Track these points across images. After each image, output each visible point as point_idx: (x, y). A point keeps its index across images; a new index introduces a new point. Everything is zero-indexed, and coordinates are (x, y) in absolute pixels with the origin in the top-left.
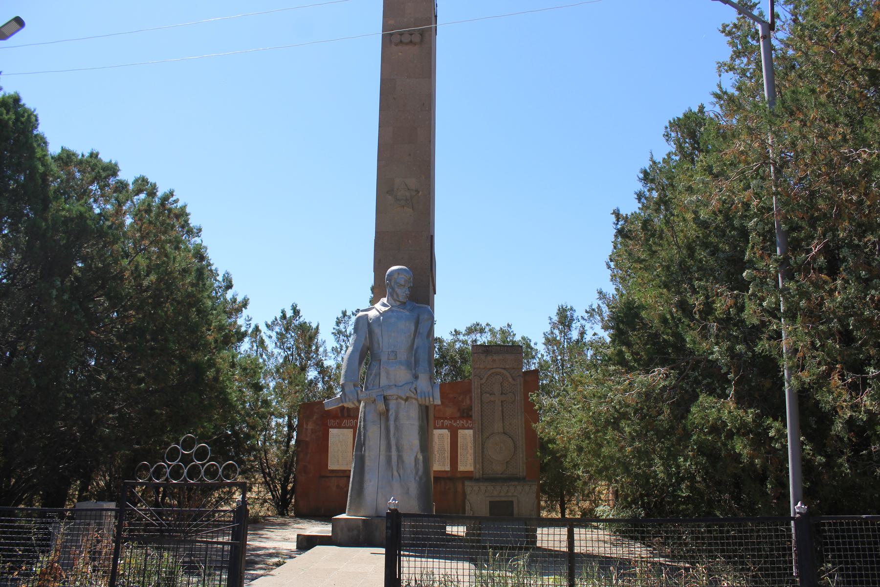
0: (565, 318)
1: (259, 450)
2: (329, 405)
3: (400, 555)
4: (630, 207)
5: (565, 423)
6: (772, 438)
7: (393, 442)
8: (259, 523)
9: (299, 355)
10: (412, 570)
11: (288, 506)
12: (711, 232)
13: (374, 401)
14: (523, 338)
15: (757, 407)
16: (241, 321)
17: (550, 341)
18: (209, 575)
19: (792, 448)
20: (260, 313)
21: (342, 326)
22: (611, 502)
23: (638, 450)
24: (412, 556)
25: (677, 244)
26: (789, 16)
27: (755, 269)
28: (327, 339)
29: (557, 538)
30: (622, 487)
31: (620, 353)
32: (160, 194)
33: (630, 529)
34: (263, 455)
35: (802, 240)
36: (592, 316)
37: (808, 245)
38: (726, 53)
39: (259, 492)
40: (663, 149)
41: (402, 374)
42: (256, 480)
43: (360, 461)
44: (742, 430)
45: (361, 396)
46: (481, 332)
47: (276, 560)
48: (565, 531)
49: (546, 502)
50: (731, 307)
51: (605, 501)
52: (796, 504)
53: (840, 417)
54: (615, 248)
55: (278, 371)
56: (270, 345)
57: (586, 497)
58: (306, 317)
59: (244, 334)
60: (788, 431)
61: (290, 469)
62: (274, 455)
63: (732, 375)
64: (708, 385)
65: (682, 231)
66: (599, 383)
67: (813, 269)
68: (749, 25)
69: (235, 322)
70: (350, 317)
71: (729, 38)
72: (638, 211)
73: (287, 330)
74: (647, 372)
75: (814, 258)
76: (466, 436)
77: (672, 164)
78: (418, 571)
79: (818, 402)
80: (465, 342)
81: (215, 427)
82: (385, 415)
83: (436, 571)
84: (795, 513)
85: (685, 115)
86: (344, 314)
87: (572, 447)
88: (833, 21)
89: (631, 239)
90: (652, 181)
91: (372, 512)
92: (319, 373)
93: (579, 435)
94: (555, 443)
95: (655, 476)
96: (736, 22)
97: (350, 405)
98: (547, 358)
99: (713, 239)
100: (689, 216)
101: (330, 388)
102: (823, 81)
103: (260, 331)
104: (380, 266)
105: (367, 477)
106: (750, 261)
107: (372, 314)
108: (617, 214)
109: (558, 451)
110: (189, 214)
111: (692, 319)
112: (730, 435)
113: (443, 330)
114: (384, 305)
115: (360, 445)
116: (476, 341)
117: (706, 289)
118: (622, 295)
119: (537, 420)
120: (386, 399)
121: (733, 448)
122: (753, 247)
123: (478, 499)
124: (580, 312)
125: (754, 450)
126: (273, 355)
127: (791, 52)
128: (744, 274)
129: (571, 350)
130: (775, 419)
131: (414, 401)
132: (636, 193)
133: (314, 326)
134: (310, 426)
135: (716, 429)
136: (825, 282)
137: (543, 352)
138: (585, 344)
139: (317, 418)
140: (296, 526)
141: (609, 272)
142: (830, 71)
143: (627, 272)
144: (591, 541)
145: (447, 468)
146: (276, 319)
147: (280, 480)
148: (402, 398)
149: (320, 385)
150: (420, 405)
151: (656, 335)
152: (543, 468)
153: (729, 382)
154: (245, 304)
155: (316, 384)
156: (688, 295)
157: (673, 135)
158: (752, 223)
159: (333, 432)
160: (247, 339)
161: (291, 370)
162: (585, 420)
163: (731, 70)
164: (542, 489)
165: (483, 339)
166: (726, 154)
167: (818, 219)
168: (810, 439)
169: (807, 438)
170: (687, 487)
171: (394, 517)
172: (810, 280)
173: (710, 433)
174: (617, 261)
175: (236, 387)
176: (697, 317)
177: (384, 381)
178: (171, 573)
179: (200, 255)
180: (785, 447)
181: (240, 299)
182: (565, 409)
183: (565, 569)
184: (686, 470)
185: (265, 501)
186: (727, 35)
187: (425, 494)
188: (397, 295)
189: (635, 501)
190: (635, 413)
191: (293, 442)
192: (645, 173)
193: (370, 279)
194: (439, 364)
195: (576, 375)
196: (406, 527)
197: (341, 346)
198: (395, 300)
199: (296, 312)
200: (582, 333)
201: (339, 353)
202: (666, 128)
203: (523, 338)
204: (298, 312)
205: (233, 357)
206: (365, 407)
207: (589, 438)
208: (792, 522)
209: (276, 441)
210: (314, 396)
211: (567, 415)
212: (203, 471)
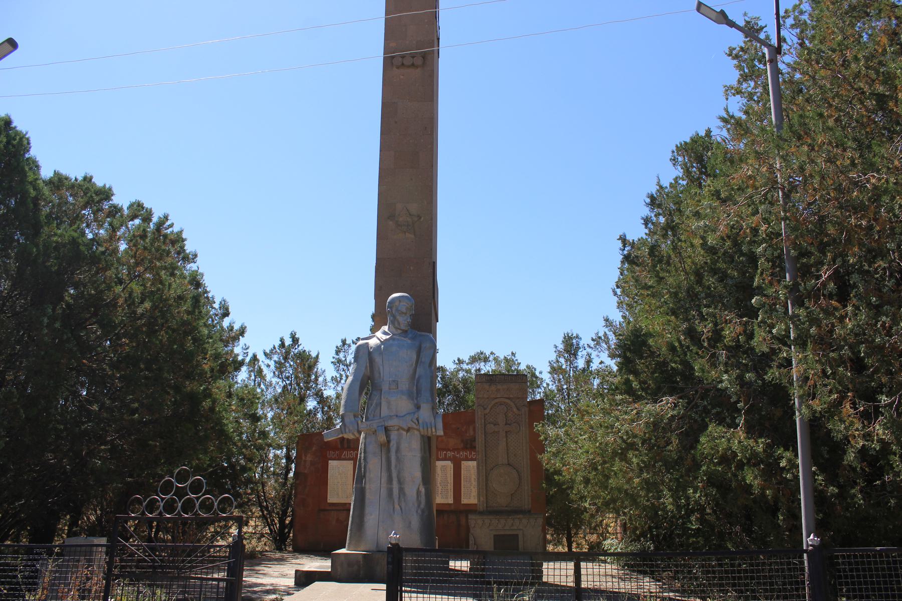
0: (570, 346)
1: (256, 483)
2: (329, 436)
3: (401, 591)
4: (637, 232)
5: (572, 451)
6: (784, 468)
7: (394, 475)
8: (256, 559)
9: (298, 385)
11: (287, 541)
12: (719, 258)
13: (375, 432)
14: (528, 367)
15: (768, 437)
16: (237, 350)
17: (555, 370)
19: (804, 479)
20: (258, 341)
21: (341, 355)
23: (646, 481)
24: (414, 592)
25: (684, 270)
26: (796, 40)
28: (326, 368)
29: (563, 572)
30: (630, 519)
31: (627, 382)
34: (260, 488)
35: (812, 266)
36: (598, 344)
37: (818, 271)
38: (732, 76)
39: (256, 526)
40: (670, 174)
41: (403, 405)
42: (253, 513)
44: (753, 460)
45: (362, 426)
49: (552, 535)
50: (740, 334)
53: (852, 447)
54: (622, 274)
55: (276, 400)
56: (269, 374)
57: (594, 530)
58: (307, 345)
59: (242, 363)
60: (799, 461)
61: (288, 502)
62: (272, 488)
64: (718, 414)
67: (824, 295)
68: (756, 49)
69: (232, 351)
70: (349, 346)
71: (735, 62)
72: (644, 237)
73: (286, 358)
74: (655, 402)
75: (824, 284)
76: (470, 467)
79: (830, 431)
80: (468, 371)
84: (808, 545)
85: (692, 139)
86: (344, 342)
87: (579, 478)
88: (839, 45)
89: (637, 265)
90: (659, 206)
91: (373, 547)
92: (318, 403)
93: (585, 467)
94: (561, 475)
96: (743, 45)
97: (351, 437)
98: (553, 387)
99: (721, 265)
100: (697, 242)
102: (831, 106)
103: (258, 361)
104: (381, 293)
105: (368, 509)
106: (759, 287)
107: (373, 342)
108: (623, 240)
109: (564, 483)
110: (185, 240)
111: (701, 347)
112: (741, 466)
113: (445, 359)
114: (385, 333)
115: (360, 478)
116: (479, 370)
118: (629, 323)
119: (542, 451)
120: (387, 430)
121: (744, 479)
122: (762, 273)
123: (483, 533)
124: (586, 340)
125: (765, 481)
126: (271, 385)
127: (798, 76)
128: (753, 301)
129: (577, 379)
130: (786, 449)
131: (416, 432)
132: (642, 218)
133: (314, 355)
134: (309, 458)
135: (726, 459)
136: (836, 309)
137: (548, 381)
139: (316, 449)
140: (294, 561)
141: (616, 299)
142: (837, 95)
143: (633, 299)
146: (274, 347)
147: (278, 513)
148: (403, 429)
149: (319, 416)
150: (422, 436)
151: (665, 364)
152: (549, 500)
153: (739, 411)
154: (242, 331)
155: (315, 415)
156: (697, 322)
157: (680, 159)
159: (332, 464)
160: (244, 369)
161: (292, 401)
162: (591, 451)
163: (738, 93)
164: (548, 522)
166: (733, 178)
168: (822, 469)
170: (697, 519)
171: (396, 552)
172: (820, 306)
173: (719, 464)
174: (623, 288)
175: (232, 417)
176: (706, 344)
177: (385, 411)
179: (196, 281)
180: (796, 478)
181: (236, 327)
184: (696, 502)
185: (262, 535)
186: (734, 58)
188: (399, 324)
189: (643, 534)
190: (643, 444)
191: (291, 475)
192: (652, 197)
193: (369, 306)
194: (441, 393)
195: (582, 405)
196: (408, 562)
197: (341, 375)
198: (396, 328)
199: (295, 340)
200: (589, 362)
201: (338, 382)
202: (673, 152)
203: (528, 367)
204: (298, 340)
205: (230, 387)
206: (365, 438)
207: (596, 469)
208: (805, 555)
209: (274, 473)
211: (573, 446)
212: (197, 505)
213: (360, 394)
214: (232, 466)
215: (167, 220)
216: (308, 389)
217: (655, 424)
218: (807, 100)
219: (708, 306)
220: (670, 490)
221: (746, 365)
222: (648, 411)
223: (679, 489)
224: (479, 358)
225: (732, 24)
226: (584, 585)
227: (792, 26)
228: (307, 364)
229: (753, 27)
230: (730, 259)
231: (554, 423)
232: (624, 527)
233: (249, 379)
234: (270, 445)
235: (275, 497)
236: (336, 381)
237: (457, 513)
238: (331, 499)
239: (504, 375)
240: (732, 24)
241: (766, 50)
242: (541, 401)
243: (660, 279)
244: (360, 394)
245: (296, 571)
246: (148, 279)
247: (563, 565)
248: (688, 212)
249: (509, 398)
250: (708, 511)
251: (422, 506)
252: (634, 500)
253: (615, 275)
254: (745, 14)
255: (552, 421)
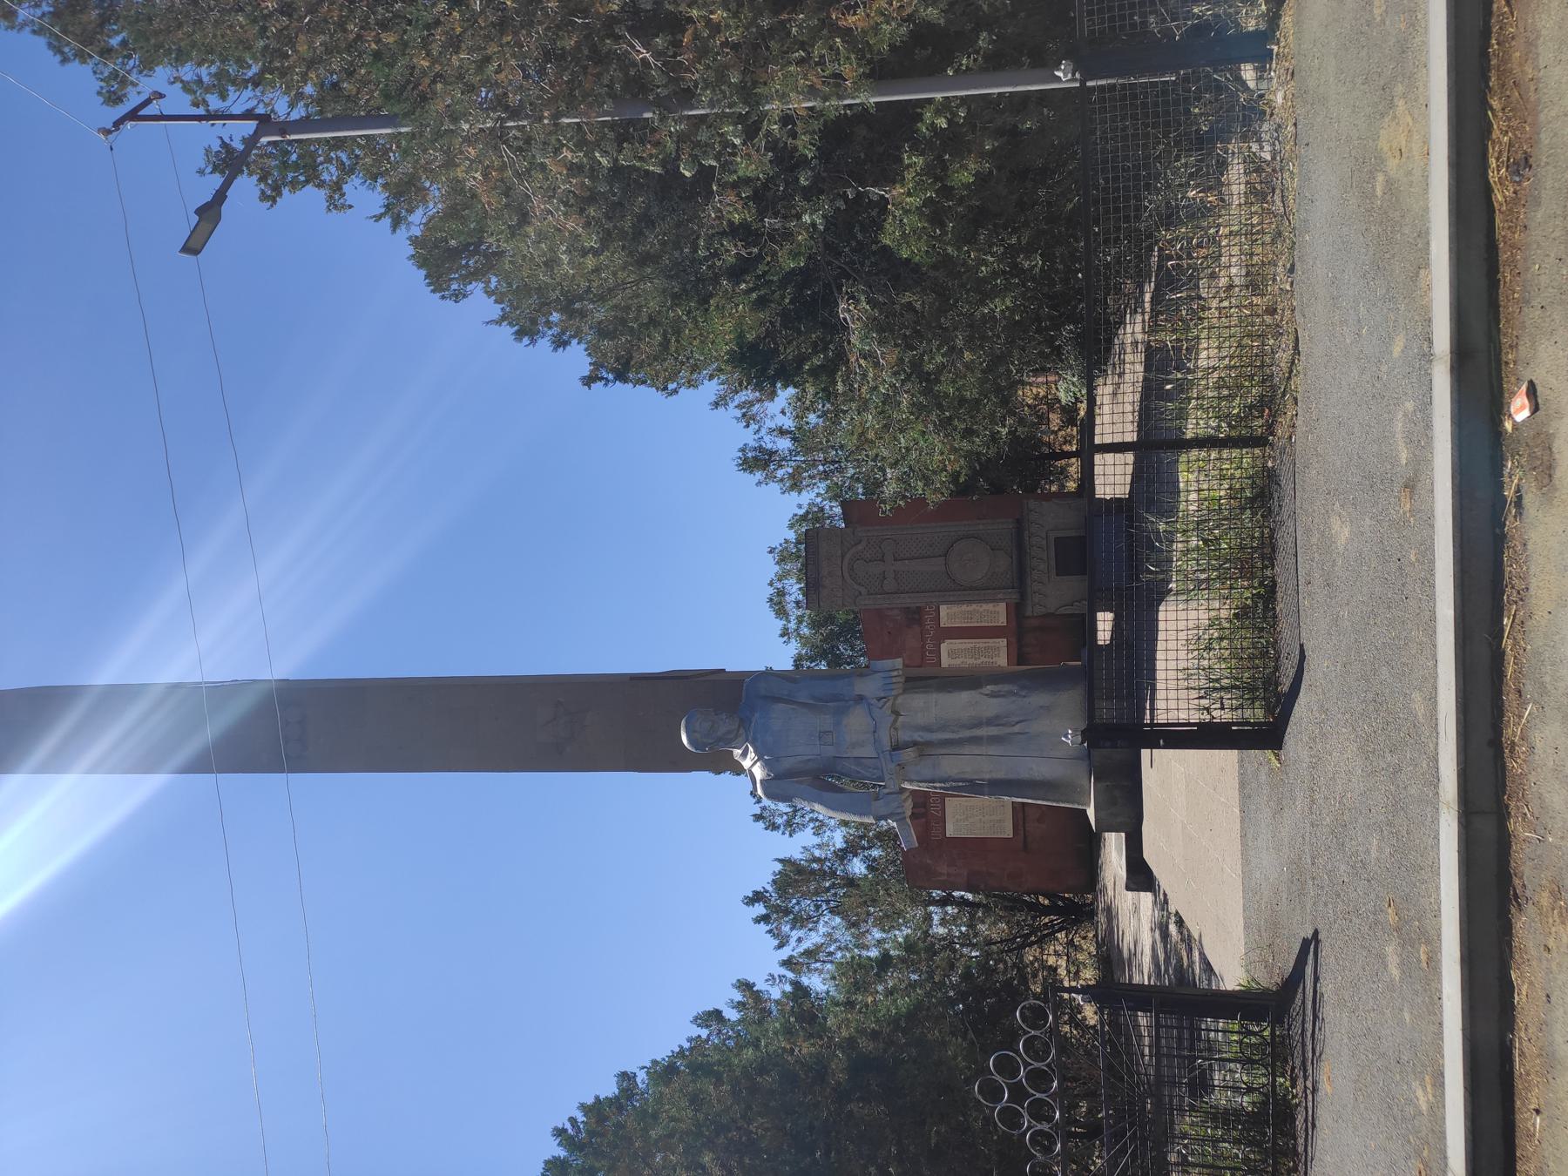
0: (758, 461)
1: (988, 955)
2: (909, 839)
3: (1152, 725)
4: (577, 358)
5: (924, 457)
6: (949, 122)
7: (967, 733)
8: (1110, 958)
9: (828, 889)
10: (1183, 705)
11: (1078, 905)
12: (615, 227)
13: (901, 766)
14: (791, 526)
15: (899, 148)
16: (776, 993)
17: (795, 484)
18: (1210, 1050)
19: (967, 89)
20: (759, 959)
21: (779, 821)
22: (1051, 378)
23: (969, 341)
24: (1152, 704)
25: (637, 283)
26: (248, 93)
27: (678, 158)
28: (799, 845)
29: (1110, 470)
30: (1028, 363)
31: (814, 372)
32: (561, 1153)
33: (1096, 355)
34: (994, 948)
35: (626, 74)
36: (753, 418)
37: (634, 64)
38: (313, 196)
39: (1056, 953)
40: (480, 304)
41: (856, 722)
42: (1036, 959)
43: (998, 787)
44: (937, 172)
45: (892, 787)
46: (783, 594)
47: (1173, 928)
48: (1098, 458)
49: (1052, 482)
50: (738, 195)
51: (1049, 388)
52: (1058, 79)
53: (916, 11)
54: (644, 382)
55: (854, 925)
56: (814, 939)
57: (1043, 419)
58: (763, 878)
59: (797, 985)
60: (938, 96)
61: (1014, 900)
62: (993, 929)
63: (849, 192)
64: (863, 229)
65: (615, 274)
66: (864, 406)
67: (675, 56)
68: (261, 156)
69: (777, 1002)
70: (764, 808)
71: (285, 191)
72: (583, 346)
73: (787, 912)
74: (846, 329)
75: (657, 55)
76: (949, 615)
77: (504, 287)
78: (1183, 694)
79: (892, 47)
80: (800, 620)
81: (953, 1034)
82: (923, 748)
83: (1182, 665)
84: (1073, 80)
85: (420, 267)
86: (758, 818)
87: (965, 445)
88: (255, 21)
89: (631, 358)
90: (534, 322)
91: (1082, 768)
92: (856, 855)
93: (946, 436)
94: (959, 473)
95: (1012, 310)
96: (255, 178)
97: (909, 804)
98: (822, 487)
99: (627, 225)
100: (590, 262)
101: (879, 836)
102: (359, 37)
103: (791, 957)
104: (680, 762)
105: (1025, 775)
106: (663, 163)
107: (758, 772)
108: (588, 381)
109: (971, 468)
110: (597, 1098)
111: (760, 258)
112: (946, 191)
113: (781, 656)
114: (744, 754)
115: (973, 787)
116: (797, 603)
117: (710, 238)
118: (720, 370)
119: (922, 501)
120: (897, 747)
121: (967, 186)
122: (641, 159)
123: (1054, 593)
124: (748, 437)
125: (970, 152)
126: (830, 934)
127: (309, 89)
128: (687, 174)
129: (808, 450)
130: (920, 118)
131: (899, 700)
132: (555, 349)
133: (779, 867)
134: (943, 869)
135: (934, 214)
136: (696, 36)
137: (813, 495)
138: (799, 428)
139: (928, 860)
140: (1110, 892)
141: (682, 390)
142: (341, 26)
143: (682, 363)
144: (1116, 417)
145: (1003, 642)
146: (770, 931)
147: (1034, 918)
148: (895, 721)
149: (875, 853)
150: (905, 691)
151: (784, 314)
152: (998, 489)
153: (859, 195)
154: (745, 986)
155: (875, 860)
156: (719, 263)
157: (454, 286)
158: (604, 161)
159: (950, 831)
160: (805, 981)
161: (856, 902)
162: (920, 427)
163: (340, 189)
164: (1031, 490)
165: (794, 589)
166: (489, 203)
167: (594, 49)
168: (948, 60)
169: (950, 64)
170: (1027, 258)
171: (1095, 735)
172: (693, 62)
173: (943, 226)
174: (667, 380)
175: (889, 998)
176: (755, 250)
177: (868, 751)
178: (1215, 1118)
179: (664, 1072)
180: (964, 99)
181: (738, 997)
182: (903, 458)
183: (1167, 456)
184: (1000, 261)
185: (1071, 943)
186: (280, 194)
187: (1050, 680)
188: (729, 732)
189: (1050, 341)
190: (913, 348)
191: (969, 896)
192: (520, 334)
193: (701, 781)
194: (836, 661)
195: (851, 442)
196: (1107, 711)
197: (812, 820)
198: (736, 737)
199: (757, 897)
200: (782, 432)
201: (823, 824)
202: (443, 297)
203: (791, 526)
204: (756, 893)
205: (837, 1004)
206: (911, 781)
207: (950, 419)
208: (1089, 84)
209: (971, 926)
210: (893, 862)
211: (914, 455)
212: (1036, 1065)
213: (841, 790)
214: (962, 996)
215: (564, 1131)
216: (833, 874)
217: (880, 330)
218: (350, 74)
219: (695, 249)
220: (982, 303)
221: (787, 184)
222: (862, 340)
223: (985, 292)
224: (778, 604)
225: (220, 196)
226: (1131, 437)
227: (223, 97)
228: (795, 877)
229: (224, 160)
230: (616, 209)
231: (879, 484)
232: (1043, 370)
233: (821, 972)
234: (926, 933)
235: (1007, 923)
236: (819, 827)
237: (1020, 632)
238: (1008, 831)
239: (805, 565)
240: (220, 196)
241: (264, 140)
242: (844, 504)
243: (653, 321)
244: (841, 790)
245: (1128, 888)
246: (664, 1159)
247: (1098, 470)
248: (547, 279)
249: (843, 557)
250: (1014, 240)
251: (1015, 689)
252: (998, 360)
253: (647, 393)
254: (201, 172)
255: (874, 486)
